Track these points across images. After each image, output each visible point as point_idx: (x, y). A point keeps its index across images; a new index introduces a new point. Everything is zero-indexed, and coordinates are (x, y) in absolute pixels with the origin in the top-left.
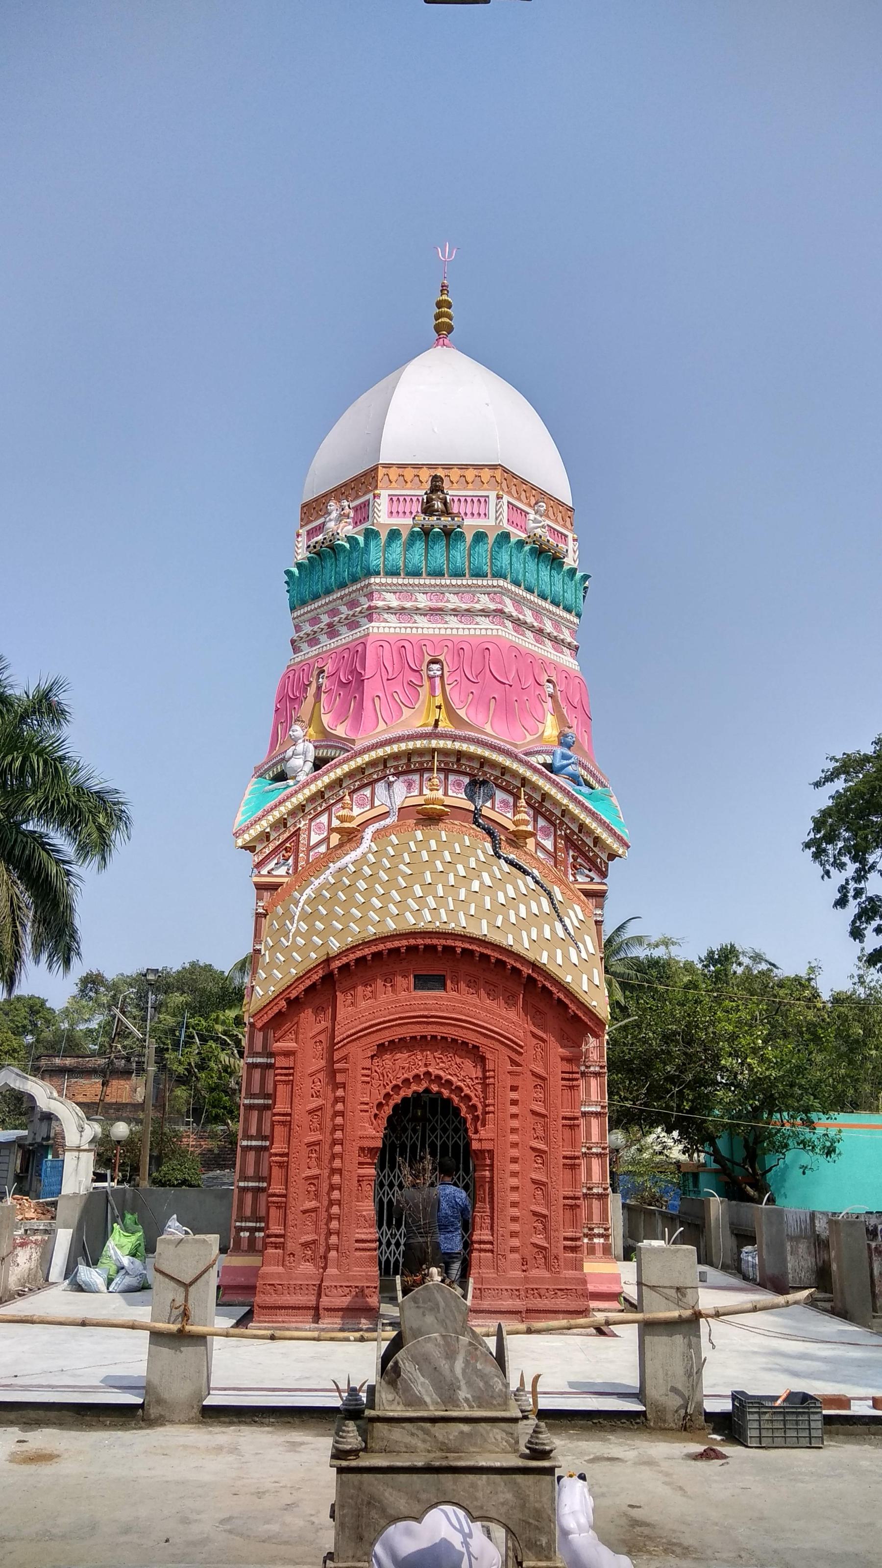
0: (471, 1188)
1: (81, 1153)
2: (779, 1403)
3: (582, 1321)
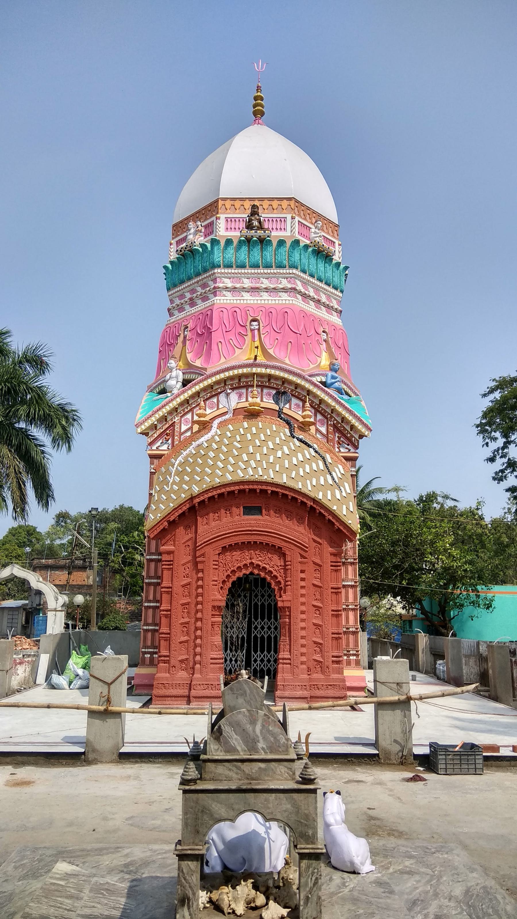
0: (279, 629)
1: (57, 612)
2: (457, 749)
3: (341, 702)
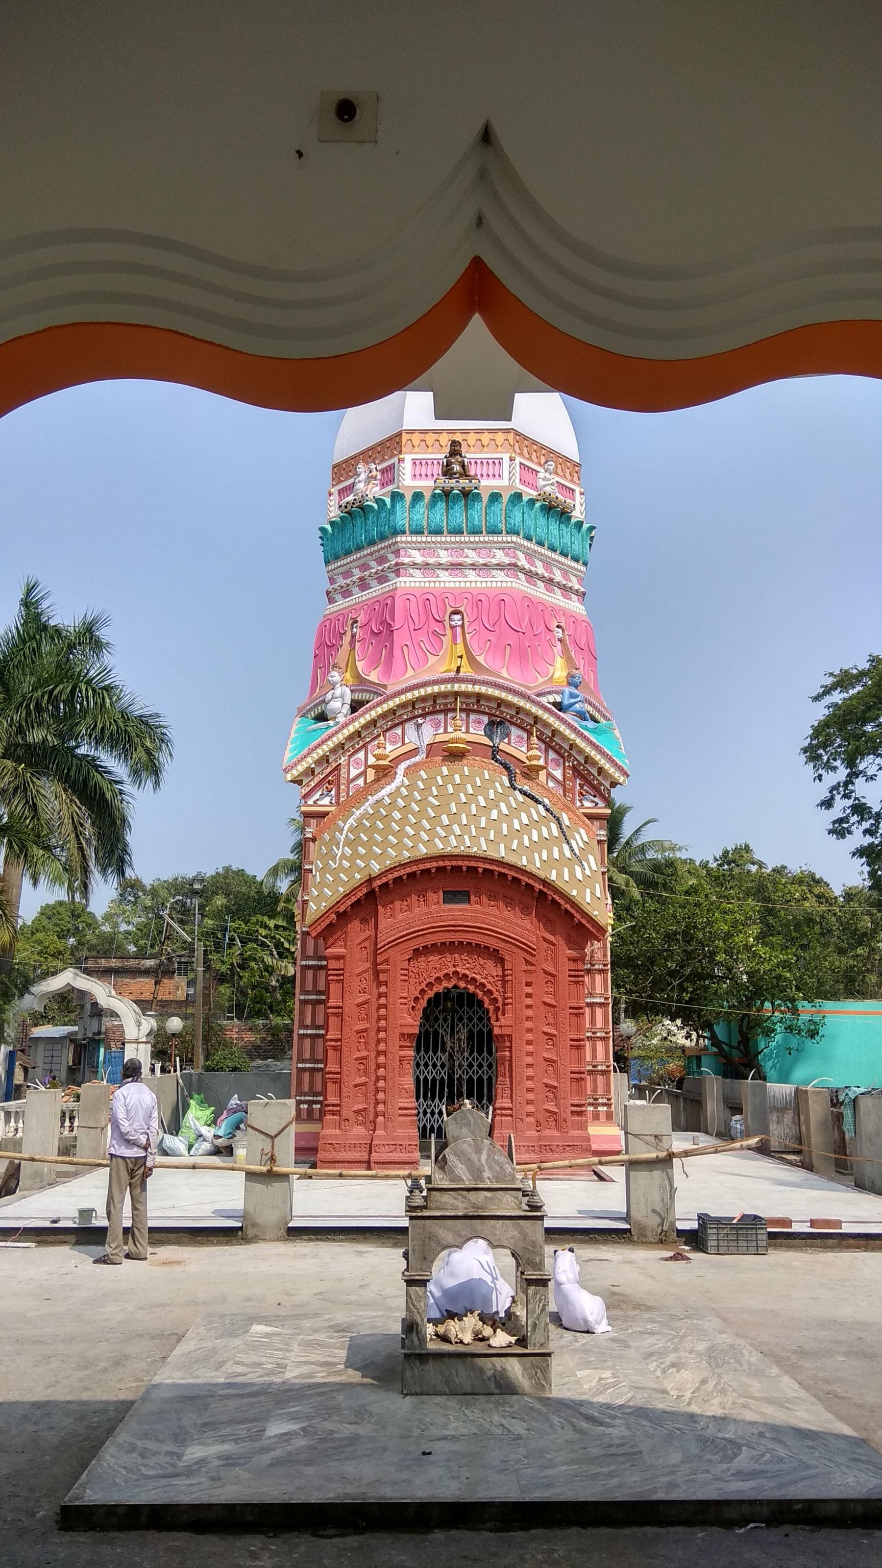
0: (494, 1067)
2: (734, 1222)
